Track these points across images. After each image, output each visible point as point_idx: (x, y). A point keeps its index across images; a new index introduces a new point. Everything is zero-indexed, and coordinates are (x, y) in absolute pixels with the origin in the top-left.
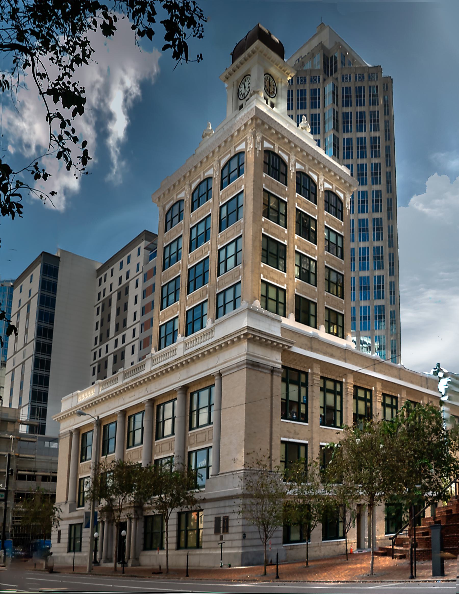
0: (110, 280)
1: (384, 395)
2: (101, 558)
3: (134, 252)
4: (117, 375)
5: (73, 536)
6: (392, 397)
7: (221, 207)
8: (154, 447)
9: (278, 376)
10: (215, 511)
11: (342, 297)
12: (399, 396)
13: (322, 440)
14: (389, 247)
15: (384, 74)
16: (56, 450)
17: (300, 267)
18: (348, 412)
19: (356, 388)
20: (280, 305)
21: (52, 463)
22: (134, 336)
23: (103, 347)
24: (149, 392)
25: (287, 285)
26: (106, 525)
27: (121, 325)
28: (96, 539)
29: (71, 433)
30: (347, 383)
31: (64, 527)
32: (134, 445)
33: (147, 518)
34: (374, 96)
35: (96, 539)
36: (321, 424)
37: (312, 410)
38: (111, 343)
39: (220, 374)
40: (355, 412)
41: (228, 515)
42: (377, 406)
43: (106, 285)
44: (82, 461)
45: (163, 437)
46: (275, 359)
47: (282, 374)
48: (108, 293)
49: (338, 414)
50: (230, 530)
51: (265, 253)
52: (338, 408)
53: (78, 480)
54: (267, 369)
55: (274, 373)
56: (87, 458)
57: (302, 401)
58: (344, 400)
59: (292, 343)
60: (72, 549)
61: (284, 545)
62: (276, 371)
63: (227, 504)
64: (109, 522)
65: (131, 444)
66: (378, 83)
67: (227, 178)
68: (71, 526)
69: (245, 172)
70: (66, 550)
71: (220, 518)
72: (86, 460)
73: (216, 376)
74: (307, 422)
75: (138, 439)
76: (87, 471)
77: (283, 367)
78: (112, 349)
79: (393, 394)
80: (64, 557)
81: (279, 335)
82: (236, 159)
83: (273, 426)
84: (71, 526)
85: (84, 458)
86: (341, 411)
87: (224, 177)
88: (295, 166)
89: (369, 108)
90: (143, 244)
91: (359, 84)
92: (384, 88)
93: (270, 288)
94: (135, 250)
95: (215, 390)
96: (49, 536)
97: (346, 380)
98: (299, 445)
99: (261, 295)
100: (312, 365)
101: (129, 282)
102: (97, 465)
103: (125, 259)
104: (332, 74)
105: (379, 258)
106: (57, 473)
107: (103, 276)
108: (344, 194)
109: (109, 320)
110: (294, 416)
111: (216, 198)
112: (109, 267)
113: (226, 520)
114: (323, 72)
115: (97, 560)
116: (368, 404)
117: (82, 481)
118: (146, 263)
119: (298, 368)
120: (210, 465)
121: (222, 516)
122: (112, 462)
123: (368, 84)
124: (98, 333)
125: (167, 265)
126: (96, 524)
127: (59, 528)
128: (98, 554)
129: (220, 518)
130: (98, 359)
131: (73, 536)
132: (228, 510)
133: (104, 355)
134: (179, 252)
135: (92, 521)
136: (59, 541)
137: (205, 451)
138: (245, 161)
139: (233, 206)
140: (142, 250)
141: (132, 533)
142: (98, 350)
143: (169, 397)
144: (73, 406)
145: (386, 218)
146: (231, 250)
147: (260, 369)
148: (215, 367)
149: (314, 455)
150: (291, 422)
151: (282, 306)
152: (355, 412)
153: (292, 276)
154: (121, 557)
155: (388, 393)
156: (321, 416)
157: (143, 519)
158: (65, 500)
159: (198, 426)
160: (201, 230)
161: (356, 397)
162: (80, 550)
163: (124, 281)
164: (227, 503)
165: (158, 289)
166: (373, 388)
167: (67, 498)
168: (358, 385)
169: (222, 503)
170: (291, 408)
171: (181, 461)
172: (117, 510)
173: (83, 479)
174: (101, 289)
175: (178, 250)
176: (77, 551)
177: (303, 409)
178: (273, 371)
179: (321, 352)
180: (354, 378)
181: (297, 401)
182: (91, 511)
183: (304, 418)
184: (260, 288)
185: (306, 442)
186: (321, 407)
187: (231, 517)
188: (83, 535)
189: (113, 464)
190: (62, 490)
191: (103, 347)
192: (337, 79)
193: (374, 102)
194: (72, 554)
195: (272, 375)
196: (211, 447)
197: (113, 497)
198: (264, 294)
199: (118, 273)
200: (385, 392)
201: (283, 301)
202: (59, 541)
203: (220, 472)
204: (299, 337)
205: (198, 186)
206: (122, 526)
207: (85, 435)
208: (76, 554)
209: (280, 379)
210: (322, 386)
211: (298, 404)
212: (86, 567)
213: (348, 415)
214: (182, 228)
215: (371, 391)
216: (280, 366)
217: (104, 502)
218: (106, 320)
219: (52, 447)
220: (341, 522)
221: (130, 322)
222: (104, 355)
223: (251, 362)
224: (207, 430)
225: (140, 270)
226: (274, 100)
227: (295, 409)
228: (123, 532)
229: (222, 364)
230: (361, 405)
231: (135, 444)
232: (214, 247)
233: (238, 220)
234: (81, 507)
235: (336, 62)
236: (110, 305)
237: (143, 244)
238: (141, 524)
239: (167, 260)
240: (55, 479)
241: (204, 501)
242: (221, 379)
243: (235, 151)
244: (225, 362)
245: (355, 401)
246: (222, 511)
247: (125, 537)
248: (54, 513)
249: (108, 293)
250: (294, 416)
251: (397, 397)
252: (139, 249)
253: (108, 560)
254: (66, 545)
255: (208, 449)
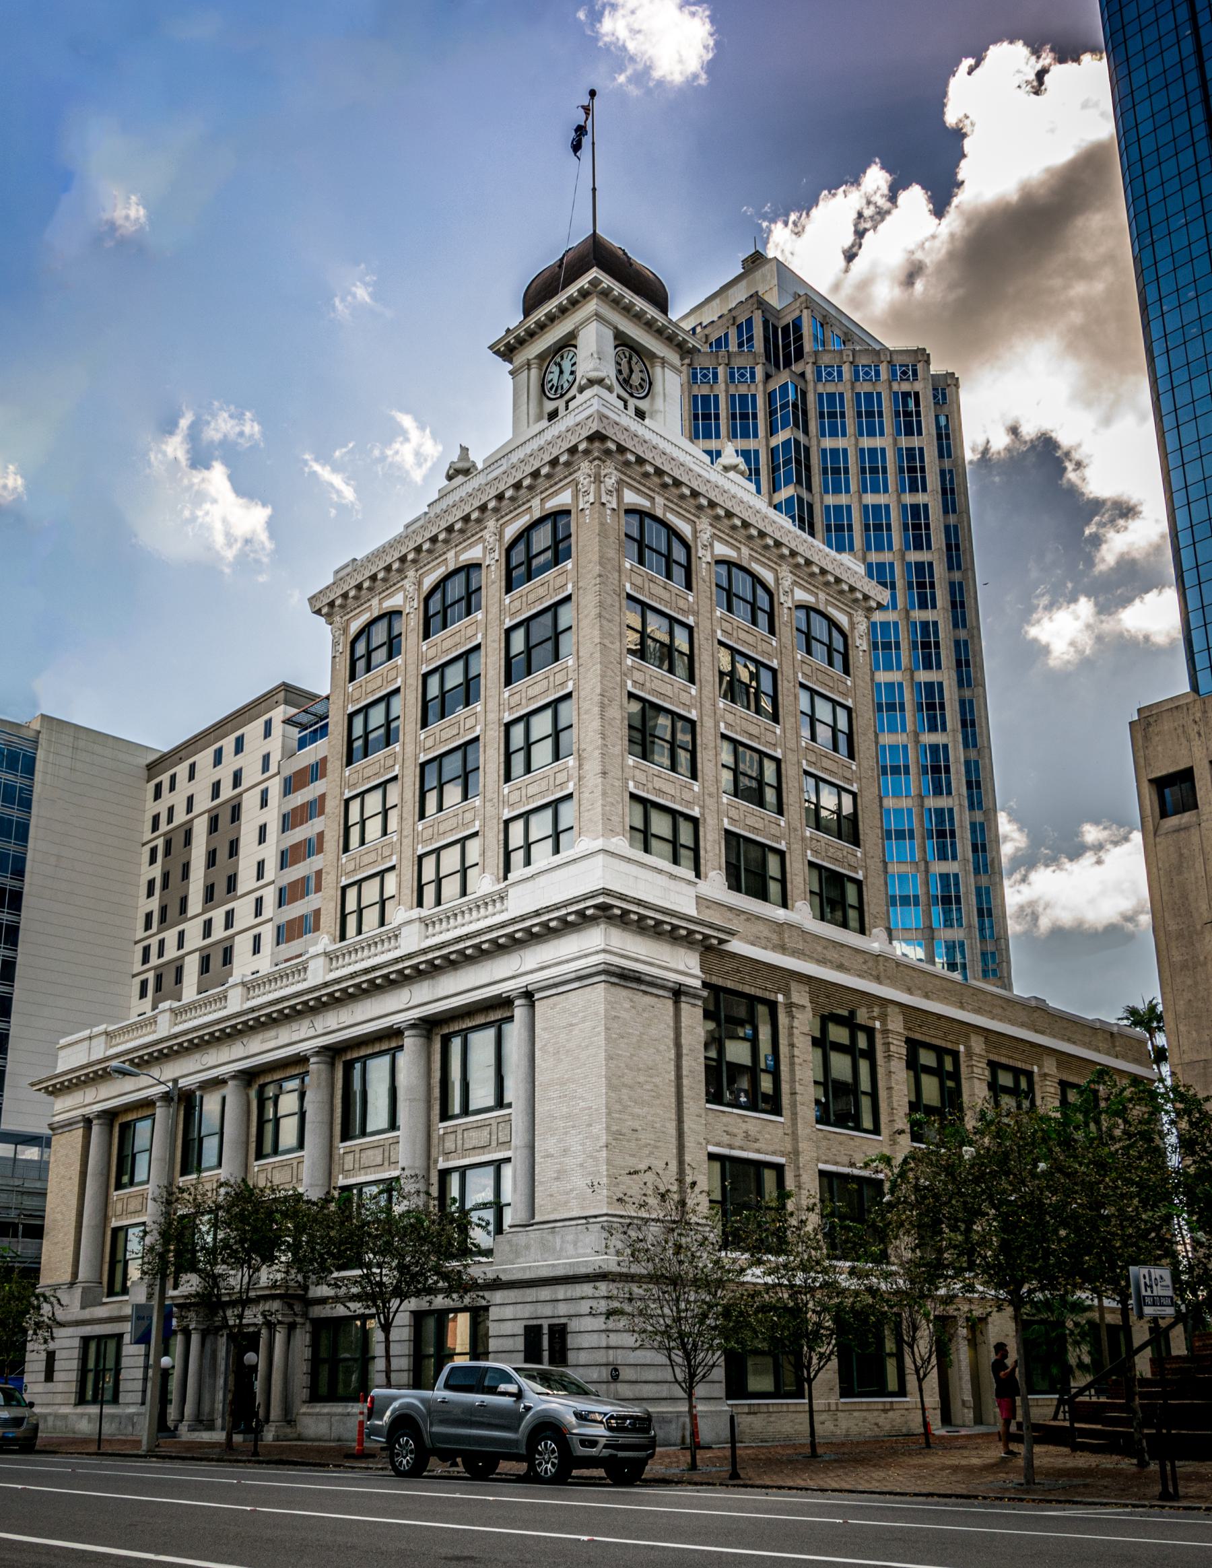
0: (185, 787)
1: (994, 1066)
2: (181, 1421)
3: (253, 730)
4: (226, 991)
5: (91, 1364)
6: (1017, 1072)
7: (508, 632)
8: (336, 1157)
9: (694, 1005)
10: (526, 1311)
11: (856, 843)
12: (1036, 1069)
13: (824, 1158)
14: (966, 746)
15: (936, 368)
16: (42, 1167)
17: (736, 771)
18: (895, 1099)
19: (913, 1046)
20: (683, 852)
21: (23, 1193)
22: (258, 912)
23: (171, 936)
24: (320, 1031)
25: (702, 807)
26: (195, 1339)
27: (223, 887)
28: (165, 1374)
29: (88, 1122)
30: (886, 1032)
31: (66, 1343)
32: (276, 1151)
33: (319, 1326)
34: (907, 414)
35: (165, 1374)
36: (818, 1122)
37: (792, 1088)
38: (193, 929)
39: (528, 995)
40: (913, 1099)
41: (563, 1321)
42: (975, 1092)
43: (177, 799)
44: (119, 1186)
45: (364, 1134)
46: (684, 966)
47: (705, 1000)
48: (180, 817)
49: (866, 1102)
50: (572, 1357)
51: (637, 736)
52: (865, 1085)
53: (109, 1233)
54: (663, 987)
55: (683, 998)
56: (137, 1179)
57: (763, 1066)
58: (881, 1071)
59: (732, 933)
60: (89, 1394)
61: (730, 1402)
62: (687, 994)
63: (561, 1296)
64: (204, 1335)
65: (268, 1147)
66: (918, 386)
67: (523, 568)
68: (86, 1340)
69: (574, 554)
70: (73, 1398)
71: (540, 1327)
72: (132, 1183)
73: (518, 997)
74: (779, 1114)
75: (288, 1135)
76: (140, 1211)
77: (705, 985)
78: (194, 939)
79: (1019, 1065)
80: (65, 1417)
81: (692, 912)
82: (547, 528)
83: (685, 1119)
84: (86, 1340)
85: (125, 1179)
86: (874, 1095)
87: (514, 564)
88: (713, 547)
89: (895, 440)
90: (279, 714)
91: (864, 388)
92: (935, 397)
93: (655, 816)
94: (258, 725)
95: (515, 1033)
96: (18, 1365)
97: (884, 1023)
98: (760, 1166)
99: (632, 828)
100: (788, 985)
101: (240, 794)
102: (170, 1198)
103: (228, 743)
104: (787, 364)
105: (937, 768)
106: (43, 1217)
107: (165, 778)
108: (850, 616)
109: (185, 875)
110: (743, 1099)
111: (494, 610)
112: (181, 760)
113: (559, 1333)
114: (762, 360)
115: (171, 1424)
116: (950, 1084)
117: (121, 1235)
118: (288, 754)
119: (747, 989)
120: (504, 1200)
121: (545, 1324)
122: (221, 1185)
123: (890, 387)
124: (154, 904)
125: (358, 752)
126: (167, 1334)
127: (52, 1346)
128: (172, 1411)
129: (540, 1327)
130: (154, 961)
131: (91, 1364)
132: (562, 1309)
133: (171, 953)
134: (393, 725)
135: (158, 1327)
136: (49, 1377)
137: (490, 1170)
138: (573, 530)
139: (541, 629)
140: (278, 728)
141: (284, 1358)
142: (154, 943)
143: (387, 1040)
144: (94, 1058)
145: (955, 683)
146: (542, 725)
147: (643, 987)
148: (513, 977)
149: (805, 1191)
150: (735, 1111)
151: (691, 854)
152: (913, 1099)
153: (713, 790)
154: (244, 1411)
155: (1004, 1060)
156: (817, 1102)
157: (308, 1327)
158: (67, 1278)
159: (466, 1111)
160: (454, 677)
161: (912, 1063)
162: (115, 1400)
163: (227, 792)
164: (561, 1292)
165: (333, 806)
166: (962, 1048)
167: (75, 1274)
168: (917, 1036)
169: (545, 1293)
170: (732, 1081)
171: (421, 1186)
172: (233, 1304)
173: (125, 1229)
174: (161, 807)
175: (388, 722)
176: (108, 1402)
177: (766, 1084)
178: (678, 993)
179: (811, 958)
180: (905, 1021)
181: (750, 1064)
182: (155, 1302)
183: (773, 1104)
184: (627, 810)
185: (782, 1160)
186: (816, 1082)
187: (573, 1325)
188: (125, 1362)
189: (222, 1191)
190: (59, 1256)
191: (171, 936)
192: (803, 375)
193: (910, 426)
194: (94, 1410)
195: (677, 1003)
196: (508, 1160)
197: (220, 1269)
198: (640, 825)
199: (207, 773)
200: (995, 1058)
201: (691, 844)
202: (49, 1377)
203: (537, 1219)
204: (748, 920)
205: (525, 535)
206: (245, 1341)
207: (127, 1130)
208: (108, 1410)
209: (699, 1012)
210: (818, 1035)
211: (753, 1071)
212: (140, 1442)
213: (895, 1105)
214: (403, 672)
215: (955, 1055)
216: (697, 983)
217: (191, 1283)
218: (173, 879)
219: (23, 1157)
220: (891, 1355)
221: (247, 880)
222: (171, 953)
223: (618, 971)
224: (492, 1121)
225: (273, 768)
226: (643, 405)
227: (744, 1083)
228: (250, 1357)
229: (532, 972)
230: (930, 1085)
231: (280, 1149)
232: (493, 717)
233: (557, 659)
234: (117, 1294)
235: (799, 338)
236: (188, 841)
237: (279, 714)
238: (302, 1338)
239: (358, 744)
240: (36, 1232)
241: (496, 1284)
242: (532, 1005)
243: (542, 509)
244: (542, 969)
245: (911, 1073)
246: (547, 1310)
247: (254, 1368)
248: (39, 1308)
249: (180, 817)
250: (743, 1099)
251: (1032, 1073)
252: (268, 724)
253: (202, 1422)
254: (73, 1387)
255: (498, 1165)
